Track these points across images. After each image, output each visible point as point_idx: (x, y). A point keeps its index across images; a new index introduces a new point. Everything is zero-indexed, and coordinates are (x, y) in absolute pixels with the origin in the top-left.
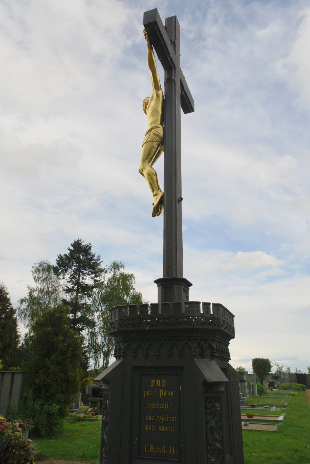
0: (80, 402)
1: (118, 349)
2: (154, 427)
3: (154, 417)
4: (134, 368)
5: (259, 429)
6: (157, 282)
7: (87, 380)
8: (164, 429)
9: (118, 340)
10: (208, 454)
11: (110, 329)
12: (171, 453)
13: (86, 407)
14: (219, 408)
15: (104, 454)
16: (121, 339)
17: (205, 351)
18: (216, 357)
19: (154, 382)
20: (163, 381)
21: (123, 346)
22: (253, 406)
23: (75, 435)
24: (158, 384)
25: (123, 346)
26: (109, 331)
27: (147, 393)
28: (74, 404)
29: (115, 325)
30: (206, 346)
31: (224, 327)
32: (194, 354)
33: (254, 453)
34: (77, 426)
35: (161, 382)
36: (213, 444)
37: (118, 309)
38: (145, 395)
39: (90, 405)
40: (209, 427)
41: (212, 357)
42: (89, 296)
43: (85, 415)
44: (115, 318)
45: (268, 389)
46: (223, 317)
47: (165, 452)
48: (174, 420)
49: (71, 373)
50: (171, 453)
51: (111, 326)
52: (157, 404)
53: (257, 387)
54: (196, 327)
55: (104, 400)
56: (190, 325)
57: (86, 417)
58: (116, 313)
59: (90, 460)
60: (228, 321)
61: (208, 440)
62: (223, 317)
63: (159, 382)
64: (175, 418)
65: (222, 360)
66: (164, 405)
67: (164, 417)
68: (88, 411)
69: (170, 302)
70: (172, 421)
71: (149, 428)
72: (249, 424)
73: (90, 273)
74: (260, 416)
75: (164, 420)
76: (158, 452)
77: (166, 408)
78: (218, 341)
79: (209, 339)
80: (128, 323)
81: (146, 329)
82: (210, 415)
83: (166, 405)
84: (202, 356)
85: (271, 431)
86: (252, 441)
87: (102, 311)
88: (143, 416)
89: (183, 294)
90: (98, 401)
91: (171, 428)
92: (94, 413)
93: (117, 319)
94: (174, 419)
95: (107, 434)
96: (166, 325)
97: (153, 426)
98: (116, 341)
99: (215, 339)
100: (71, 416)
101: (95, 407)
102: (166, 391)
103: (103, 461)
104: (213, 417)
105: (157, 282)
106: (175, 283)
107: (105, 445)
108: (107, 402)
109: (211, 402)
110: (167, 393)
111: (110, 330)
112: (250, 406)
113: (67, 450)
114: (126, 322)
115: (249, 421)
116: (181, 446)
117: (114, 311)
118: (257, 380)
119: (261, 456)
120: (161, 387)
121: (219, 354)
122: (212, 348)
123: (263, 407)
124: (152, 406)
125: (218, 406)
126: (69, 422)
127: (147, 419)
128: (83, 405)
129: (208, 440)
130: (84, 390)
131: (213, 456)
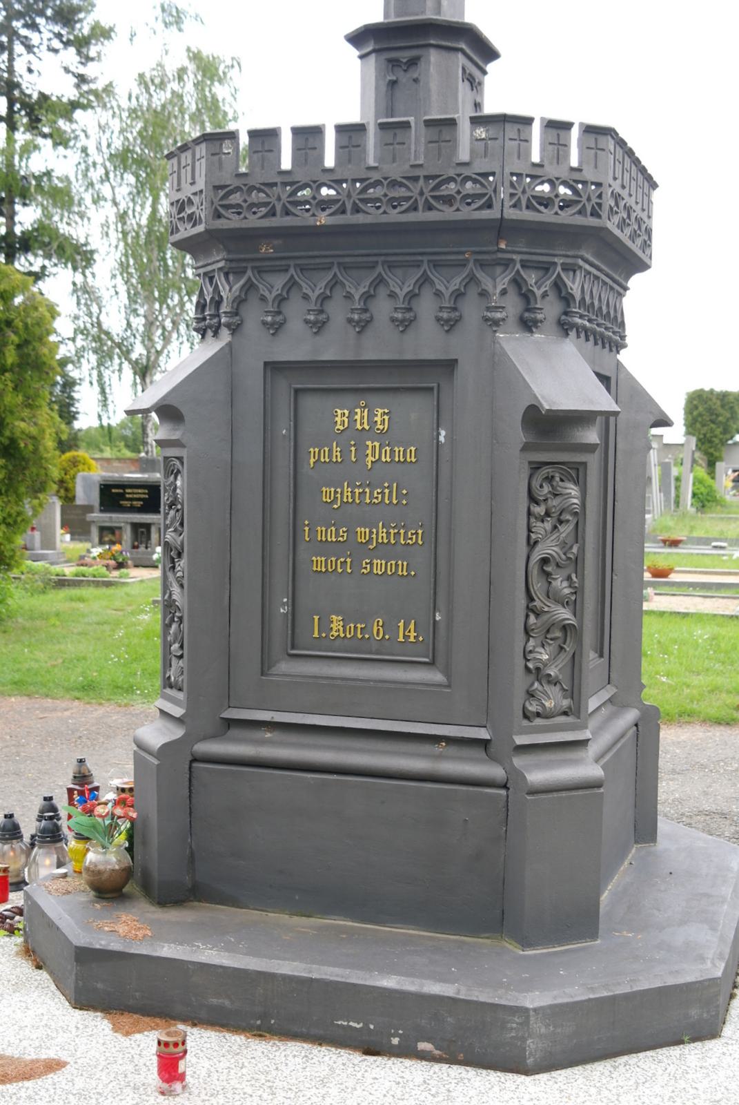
0: (59, 531)
1: (208, 301)
2: (345, 562)
3: (345, 529)
4: (274, 368)
5: (686, 608)
6: (357, 39)
7: (74, 457)
8: (379, 566)
9: (209, 268)
10: (528, 641)
11: (177, 228)
12: (401, 639)
13: (80, 547)
14: (575, 501)
15: (176, 646)
16: (221, 264)
17: (538, 306)
18: (579, 330)
19: (347, 415)
20: (381, 411)
21: (227, 288)
22: (675, 543)
23: (54, 625)
24: (362, 424)
25: (230, 290)
26: (172, 233)
27: (319, 451)
28: (37, 534)
29: (194, 209)
30: (543, 289)
31: (616, 219)
32: (498, 315)
33: (663, 676)
34: (57, 600)
35: (371, 415)
36: (546, 609)
37: (203, 146)
38: (312, 460)
39: (96, 540)
40: (536, 556)
41: (564, 328)
42: (61, 140)
43: (82, 568)
44: (193, 184)
45: (732, 493)
46: (615, 179)
47: (383, 637)
48: (417, 538)
49: (23, 425)
50: (401, 639)
51: (179, 213)
52: (357, 490)
53: (694, 484)
54: (511, 214)
55: (167, 476)
56: (489, 205)
57: (84, 576)
58: (197, 164)
59: (112, 697)
60: (633, 198)
61: (530, 598)
62: (615, 179)
63: (366, 414)
64: (420, 532)
65: (596, 344)
66: (383, 493)
67: (381, 531)
68: (89, 557)
69: (413, 118)
70: (409, 541)
71: (326, 566)
72: (656, 594)
73: (56, 44)
74: (695, 572)
75: (380, 538)
76: (360, 636)
77: (387, 502)
78: (589, 273)
79: (555, 264)
80: (245, 201)
81: (318, 223)
82: (543, 521)
83: (387, 491)
84: (528, 325)
85: (727, 616)
86: (659, 642)
87: (115, 203)
88: (307, 529)
89: (463, 88)
90: (122, 525)
91: (405, 563)
92: (112, 563)
93: (201, 184)
94: (414, 537)
95: (182, 586)
96: (395, 207)
97: (342, 560)
98: (201, 271)
99: (581, 262)
100: (32, 572)
101: (112, 543)
102: (388, 445)
103: (171, 666)
104: (555, 527)
105: (357, 39)
106: (432, 42)
107: (176, 619)
108: (179, 483)
109: (549, 479)
110: (392, 451)
111: (178, 230)
112: (664, 541)
113: (28, 670)
114: (236, 198)
115: (655, 588)
116: (438, 618)
117: (188, 154)
118: (694, 461)
119: (684, 684)
120: (371, 433)
121: (589, 321)
122: (566, 299)
123: (708, 545)
124: (339, 495)
125: (573, 493)
126: (26, 589)
127: (319, 539)
128: (72, 539)
129: (530, 598)
130: (67, 490)
131: (543, 646)
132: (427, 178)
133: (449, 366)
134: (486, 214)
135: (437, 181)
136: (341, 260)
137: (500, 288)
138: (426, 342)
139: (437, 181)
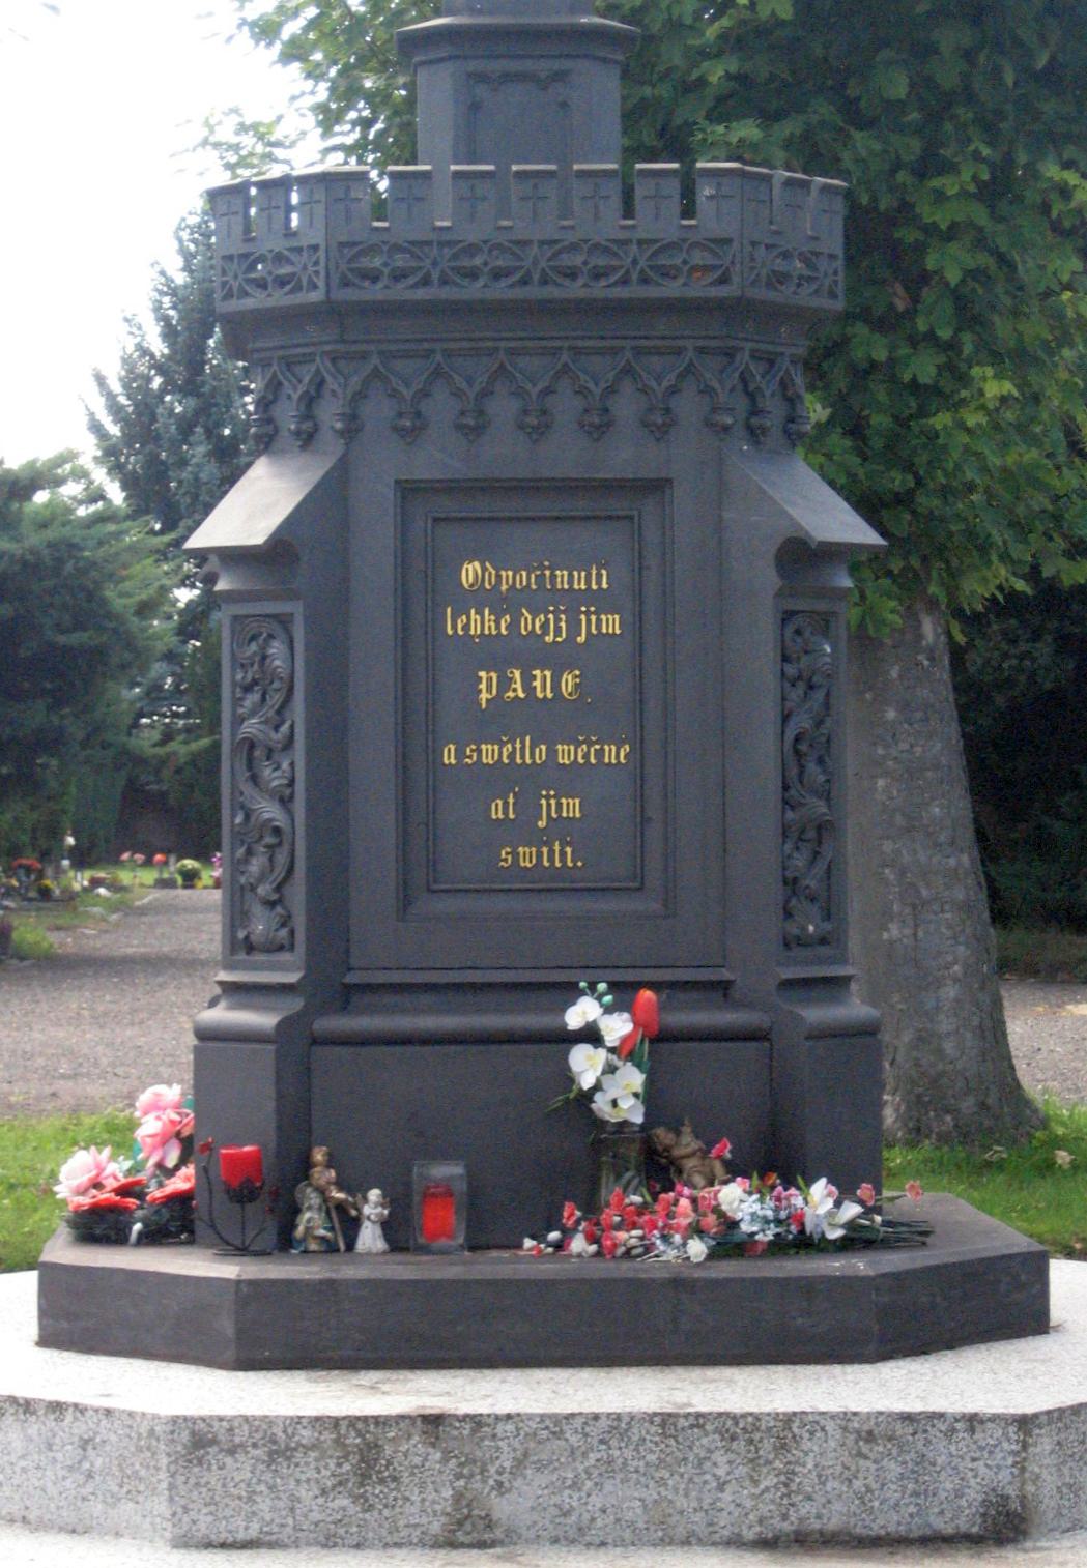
4: (408, 490)
132: (640, 243)
133: (658, 486)
134: (723, 292)
135: (356, 249)
136: (445, 345)
137: (728, 386)
138: (624, 456)
139: (356, 249)
